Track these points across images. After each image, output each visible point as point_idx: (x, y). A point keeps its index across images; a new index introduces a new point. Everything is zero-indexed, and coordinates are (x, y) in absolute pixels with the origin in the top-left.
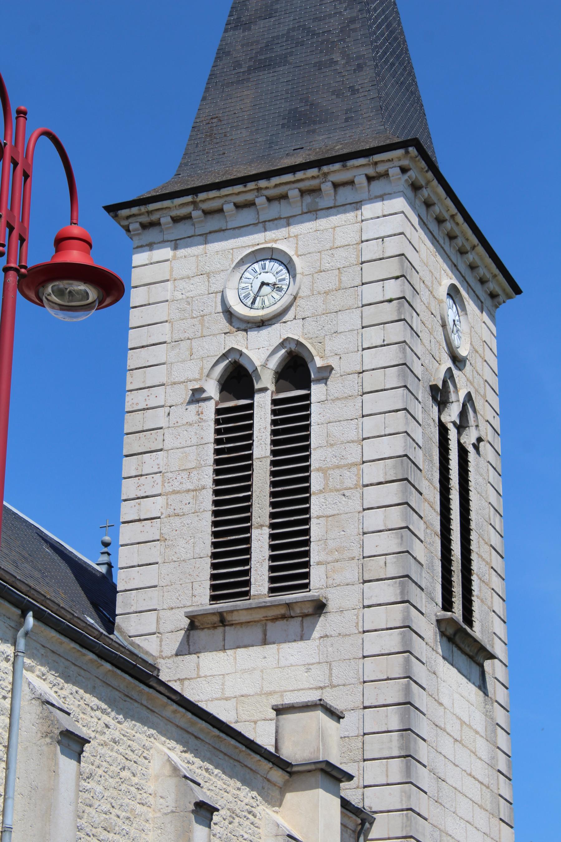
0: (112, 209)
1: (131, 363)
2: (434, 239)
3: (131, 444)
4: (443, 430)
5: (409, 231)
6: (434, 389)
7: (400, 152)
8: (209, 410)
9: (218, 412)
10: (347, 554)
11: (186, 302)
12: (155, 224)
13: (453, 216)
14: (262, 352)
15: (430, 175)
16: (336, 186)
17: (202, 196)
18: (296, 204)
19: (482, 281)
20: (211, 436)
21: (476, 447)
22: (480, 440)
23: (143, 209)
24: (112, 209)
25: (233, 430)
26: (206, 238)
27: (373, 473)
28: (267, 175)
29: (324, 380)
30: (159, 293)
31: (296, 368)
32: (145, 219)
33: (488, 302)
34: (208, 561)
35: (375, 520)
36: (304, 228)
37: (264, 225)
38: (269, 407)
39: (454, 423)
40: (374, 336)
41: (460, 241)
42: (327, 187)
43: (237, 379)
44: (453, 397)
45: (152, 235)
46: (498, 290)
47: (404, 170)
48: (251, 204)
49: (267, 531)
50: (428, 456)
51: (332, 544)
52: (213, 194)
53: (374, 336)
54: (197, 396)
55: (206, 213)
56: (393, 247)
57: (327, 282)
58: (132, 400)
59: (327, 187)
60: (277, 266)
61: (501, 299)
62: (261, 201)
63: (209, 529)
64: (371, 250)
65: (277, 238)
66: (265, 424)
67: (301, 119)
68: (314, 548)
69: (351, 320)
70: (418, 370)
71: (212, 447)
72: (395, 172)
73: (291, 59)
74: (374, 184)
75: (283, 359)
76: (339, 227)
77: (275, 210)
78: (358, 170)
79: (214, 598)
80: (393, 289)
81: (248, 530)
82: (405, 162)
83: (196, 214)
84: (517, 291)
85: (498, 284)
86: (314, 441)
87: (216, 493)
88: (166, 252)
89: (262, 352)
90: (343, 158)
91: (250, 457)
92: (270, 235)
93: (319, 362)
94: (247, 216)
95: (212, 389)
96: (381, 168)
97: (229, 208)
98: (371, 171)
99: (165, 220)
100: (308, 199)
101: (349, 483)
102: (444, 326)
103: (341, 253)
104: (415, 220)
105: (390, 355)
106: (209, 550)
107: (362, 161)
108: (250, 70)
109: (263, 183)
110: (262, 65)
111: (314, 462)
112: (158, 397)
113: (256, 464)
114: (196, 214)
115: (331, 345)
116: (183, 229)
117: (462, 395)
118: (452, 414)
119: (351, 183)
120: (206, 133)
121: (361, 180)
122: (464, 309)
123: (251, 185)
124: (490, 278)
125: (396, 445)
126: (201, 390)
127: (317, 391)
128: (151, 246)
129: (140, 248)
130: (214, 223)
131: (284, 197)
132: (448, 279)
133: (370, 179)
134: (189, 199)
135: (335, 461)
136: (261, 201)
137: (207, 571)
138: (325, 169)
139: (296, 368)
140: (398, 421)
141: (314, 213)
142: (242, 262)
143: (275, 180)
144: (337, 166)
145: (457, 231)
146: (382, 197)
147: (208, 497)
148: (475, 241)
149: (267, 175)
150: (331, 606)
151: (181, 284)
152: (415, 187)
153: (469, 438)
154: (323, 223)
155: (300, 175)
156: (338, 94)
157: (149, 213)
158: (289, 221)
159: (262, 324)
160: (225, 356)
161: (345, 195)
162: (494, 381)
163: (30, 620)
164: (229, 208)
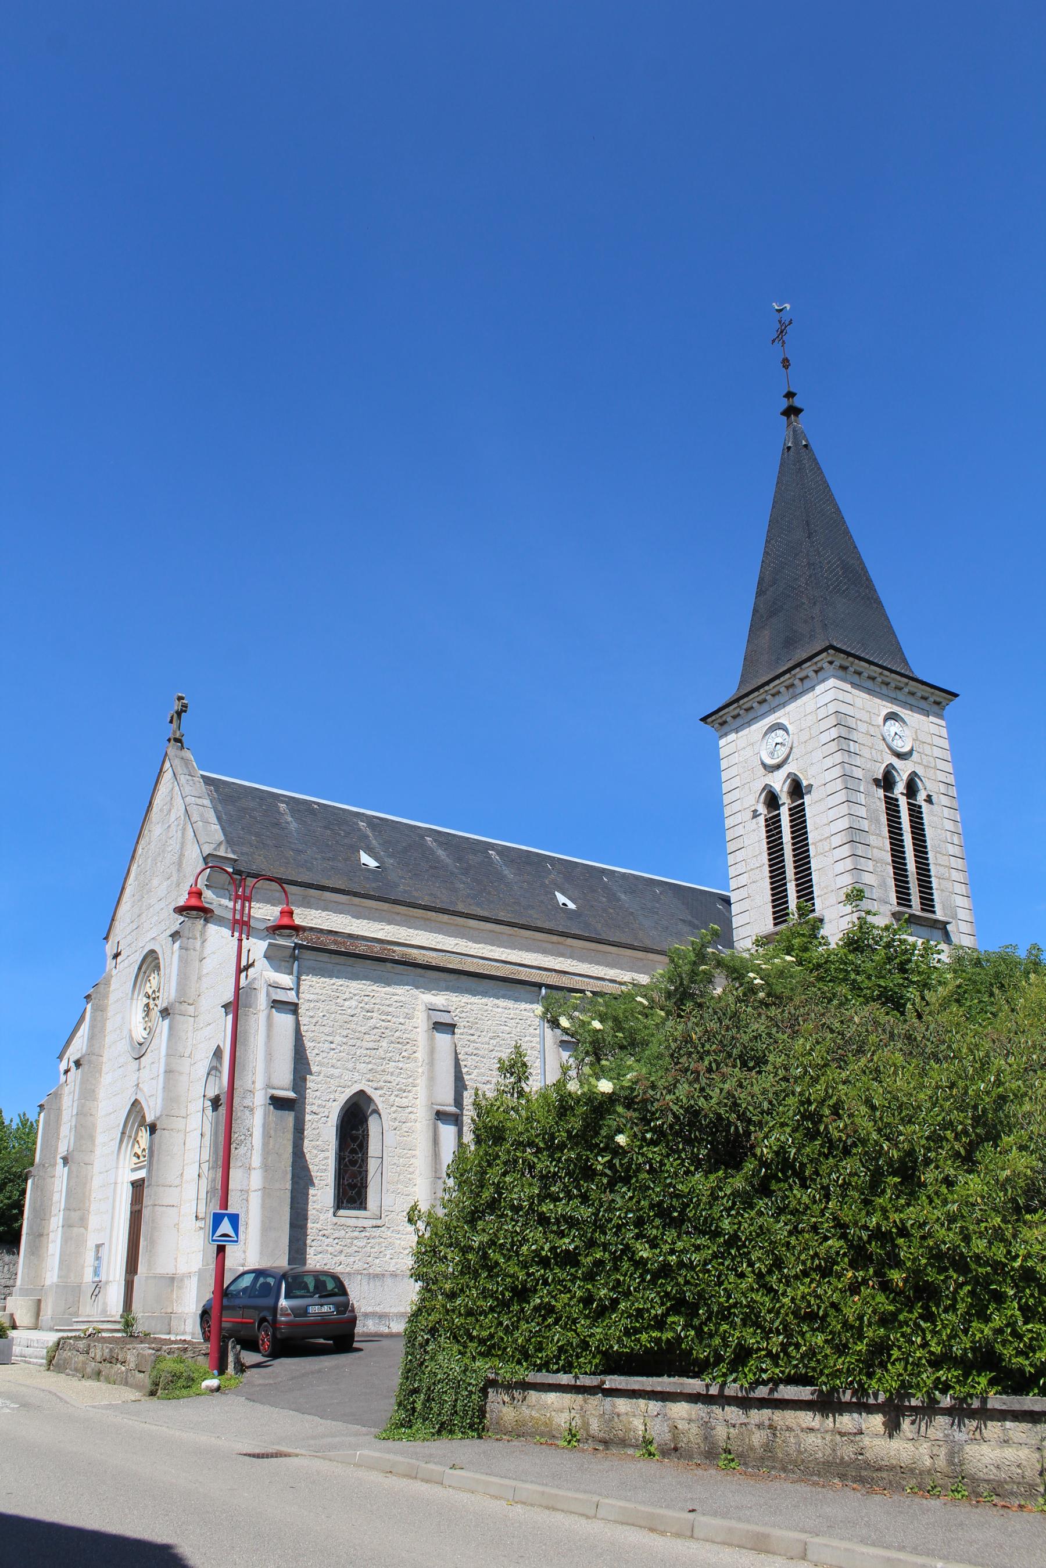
0: (704, 719)
1: (725, 802)
2: (869, 691)
3: (731, 847)
4: (892, 806)
5: (841, 696)
6: (876, 782)
7: (825, 654)
8: (761, 820)
9: (790, 809)
10: (830, 889)
11: (746, 758)
12: (725, 722)
13: (881, 674)
14: (779, 783)
15: (851, 659)
16: (802, 680)
17: (741, 702)
18: (785, 695)
19: (925, 698)
20: (764, 835)
21: (929, 800)
22: (929, 796)
23: (717, 716)
24: (701, 720)
25: (773, 826)
26: (749, 723)
27: (837, 840)
28: (767, 683)
29: (809, 792)
30: (735, 758)
31: (797, 789)
32: (720, 721)
33: (936, 708)
34: (771, 904)
35: (841, 867)
36: (791, 707)
37: (773, 710)
38: (787, 813)
39: (902, 794)
40: (829, 762)
41: (893, 685)
42: (797, 682)
43: (772, 801)
44: (898, 779)
45: (726, 728)
46: (938, 699)
47: (831, 663)
48: (765, 701)
49: (794, 883)
50: (873, 819)
51: (823, 885)
52: (746, 700)
53: (829, 762)
54: (755, 815)
55: (747, 710)
56: (832, 708)
57: (805, 736)
58: (728, 823)
59: (797, 682)
60: (780, 732)
61: (944, 704)
62: (769, 697)
63: (769, 887)
64: (822, 713)
65: (779, 717)
66: (786, 815)
67: (790, 642)
68: (815, 888)
69: (818, 754)
70: (858, 773)
71: (765, 841)
72: (826, 665)
73: (785, 607)
74: (819, 674)
75: (791, 784)
76: (807, 703)
77: (778, 700)
78: (808, 669)
79: (775, 925)
80: (834, 733)
81: (785, 884)
82: (830, 659)
83: (742, 712)
84: (956, 695)
85: (939, 696)
86: (809, 829)
87: (770, 866)
88: (732, 736)
89: (779, 783)
90: (799, 665)
91: (782, 843)
92: (777, 714)
93: (805, 783)
94: (765, 707)
95: (762, 809)
96: (819, 665)
97: (755, 705)
98: (815, 668)
99: (729, 719)
100: (791, 690)
101: (827, 848)
102: (884, 739)
103: (810, 717)
104: (848, 687)
105: (837, 772)
106: (770, 898)
107: (809, 664)
108: (767, 619)
109: (767, 688)
110: (773, 613)
111: (810, 841)
112: (738, 819)
113: (785, 846)
114: (742, 712)
115: (812, 771)
116: (739, 721)
117: (905, 777)
118: (900, 788)
119: (807, 677)
120: (750, 661)
121: (812, 674)
122: (904, 722)
123: (762, 691)
124: (935, 698)
125: (844, 823)
126: (755, 811)
127: (807, 799)
128: (726, 735)
129: (721, 737)
130: (751, 715)
131: (779, 692)
132: (887, 708)
133: (816, 672)
134: (735, 705)
135: (820, 838)
136: (769, 697)
137: (771, 910)
138: (793, 672)
139: (797, 789)
140: (844, 809)
141: (794, 697)
142: (766, 734)
143: (772, 685)
144: (798, 670)
145: (887, 680)
146: (823, 681)
147: (767, 869)
148: (906, 680)
149: (767, 683)
150: (826, 920)
151: (741, 753)
152: (844, 668)
153: (921, 796)
154: (800, 702)
155: (782, 679)
156: (806, 622)
157: (721, 717)
158: (784, 705)
159: (778, 767)
160: (764, 789)
161: (807, 684)
162: (948, 755)
163: (543, 991)
164: (755, 705)
